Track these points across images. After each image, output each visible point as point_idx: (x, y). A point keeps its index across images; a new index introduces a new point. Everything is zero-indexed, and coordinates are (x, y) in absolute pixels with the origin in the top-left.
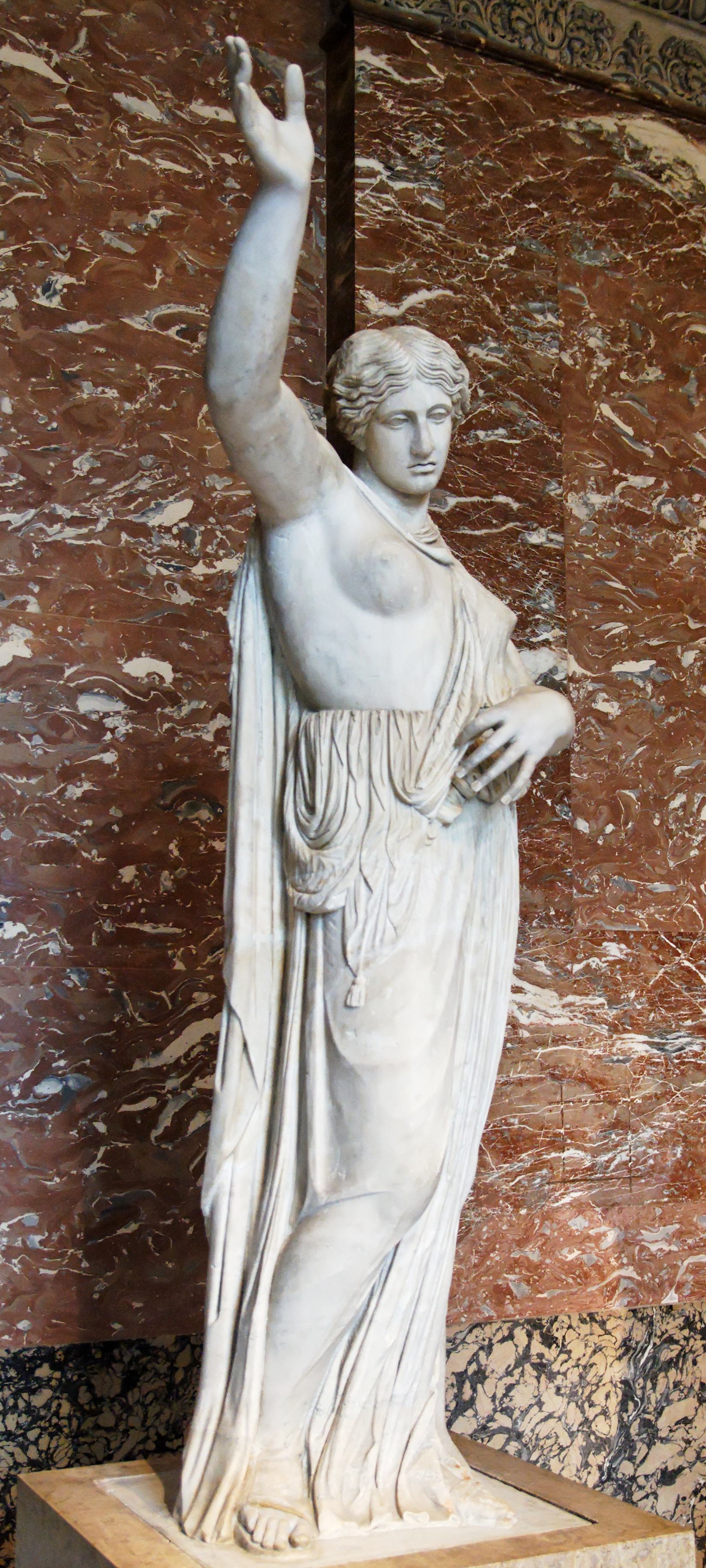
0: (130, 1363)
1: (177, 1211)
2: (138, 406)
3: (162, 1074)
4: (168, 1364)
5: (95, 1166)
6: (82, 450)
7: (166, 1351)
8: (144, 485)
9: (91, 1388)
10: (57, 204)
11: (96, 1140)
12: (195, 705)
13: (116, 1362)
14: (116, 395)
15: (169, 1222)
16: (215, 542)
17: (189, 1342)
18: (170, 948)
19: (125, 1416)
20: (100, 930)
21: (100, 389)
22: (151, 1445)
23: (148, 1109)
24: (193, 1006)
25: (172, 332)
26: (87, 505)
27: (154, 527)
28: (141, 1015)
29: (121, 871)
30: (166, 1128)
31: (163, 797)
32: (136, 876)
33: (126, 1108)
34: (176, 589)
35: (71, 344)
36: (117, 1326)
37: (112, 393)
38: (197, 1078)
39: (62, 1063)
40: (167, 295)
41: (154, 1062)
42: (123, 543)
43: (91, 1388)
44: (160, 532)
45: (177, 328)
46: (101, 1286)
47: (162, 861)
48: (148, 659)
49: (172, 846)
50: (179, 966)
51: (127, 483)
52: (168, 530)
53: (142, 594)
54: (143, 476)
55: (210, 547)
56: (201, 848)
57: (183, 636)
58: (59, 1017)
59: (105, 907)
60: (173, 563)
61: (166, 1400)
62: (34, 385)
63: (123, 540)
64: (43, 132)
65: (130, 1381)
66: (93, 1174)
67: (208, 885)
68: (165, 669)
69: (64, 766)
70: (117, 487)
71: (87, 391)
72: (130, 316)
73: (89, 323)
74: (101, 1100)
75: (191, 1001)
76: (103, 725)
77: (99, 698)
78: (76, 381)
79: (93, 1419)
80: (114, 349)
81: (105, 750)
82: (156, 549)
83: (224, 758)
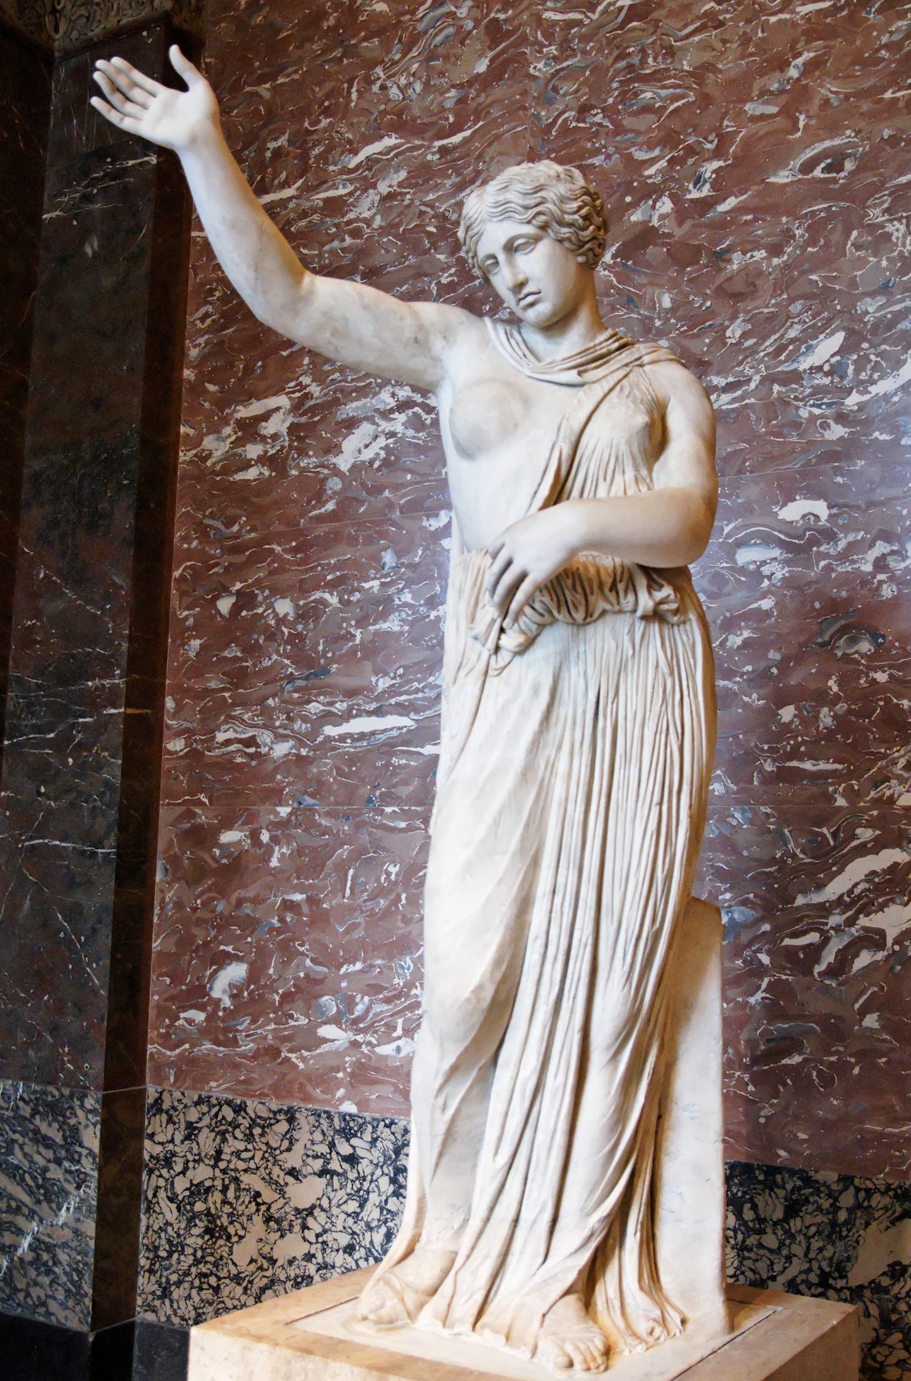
0: (792, 1191)
1: (842, 1049)
2: (785, 257)
3: (824, 909)
4: (831, 1201)
5: (759, 995)
6: (734, 318)
7: (828, 1187)
8: (792, 334)
9: (754, 1207)
10: (705, 100)
11: (758, 971)
12: (851, 537)
13: (778, 1187)
14: (765, 254)
15: (834, 1059)
16: (869, 367)
17: (852, 1183)
18: (831, 784)
19: (787, 1242)
20: (761, 770)
21: (749, 255)
22: (813, 1278)
23: (811, 944)
24: (855, 843)
25: (818, 173)
26: (741, 368)
27: (805, 371)
28: (803, 852)
29: (780, 712)
30: (829, 964)
31: (821, 633)
32: (795, 716)
33: (787, 942)
34: (829, 426)
35: (722, 225)
36: (782, 1153)
37: (760, 254)
38: (861, 916)
39: (728, 896)
40: (812, 137)
41: (817, 898)
42: (775, 395)
43: (754, 1207)
44: (811, 373)
45: (823, 165)
46: (767, 1111)
47: (822, 697)
48: (803, 501)
49: (831, 683)
50: (841, 802)
51: (778, 335)
52: (820, 369)
53: (795, 439)
54: (792, 323)
55: (863, 374)
56: (862, 681)
57: (838, 471)
58: (723, 853)
59: (766, 747)
60: (825, 400)
61: (829, 1236)
62: (691, 272)
63: (775, 391)
64: (691, 40)
65: (792, 1210)
66: (757, 1003)
67: (869, 718)
68: (820, 508)
69: (725, 617)
70: (767, 343)
71: (737, 260)
72: (775, 175)
73: (736, 197)
74: (764, 933)
75: (854, 837)
76: (761, 573)
77: (756, 548)
78: (727, 256)
79: (757, 1237)
80: (759, 211)
81: (763, 596)
82: (808, 391)
83: (885, 586)
